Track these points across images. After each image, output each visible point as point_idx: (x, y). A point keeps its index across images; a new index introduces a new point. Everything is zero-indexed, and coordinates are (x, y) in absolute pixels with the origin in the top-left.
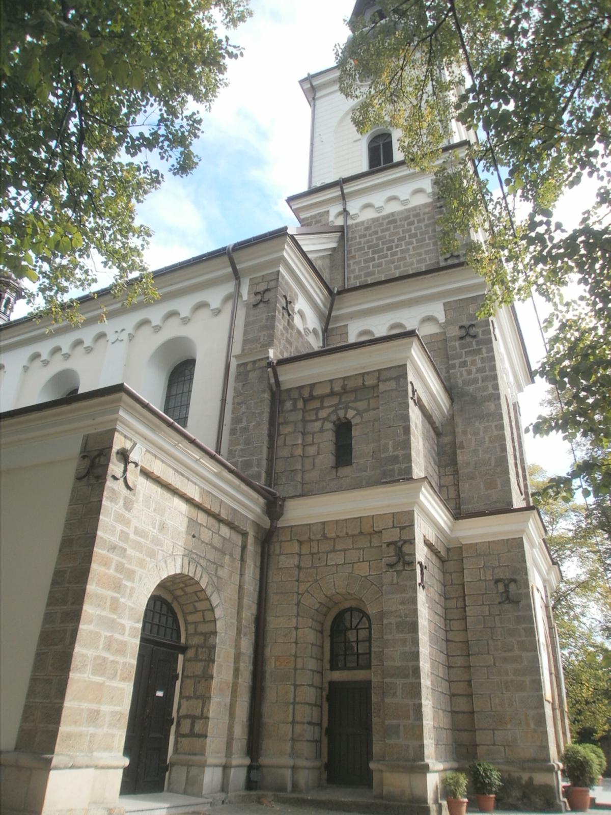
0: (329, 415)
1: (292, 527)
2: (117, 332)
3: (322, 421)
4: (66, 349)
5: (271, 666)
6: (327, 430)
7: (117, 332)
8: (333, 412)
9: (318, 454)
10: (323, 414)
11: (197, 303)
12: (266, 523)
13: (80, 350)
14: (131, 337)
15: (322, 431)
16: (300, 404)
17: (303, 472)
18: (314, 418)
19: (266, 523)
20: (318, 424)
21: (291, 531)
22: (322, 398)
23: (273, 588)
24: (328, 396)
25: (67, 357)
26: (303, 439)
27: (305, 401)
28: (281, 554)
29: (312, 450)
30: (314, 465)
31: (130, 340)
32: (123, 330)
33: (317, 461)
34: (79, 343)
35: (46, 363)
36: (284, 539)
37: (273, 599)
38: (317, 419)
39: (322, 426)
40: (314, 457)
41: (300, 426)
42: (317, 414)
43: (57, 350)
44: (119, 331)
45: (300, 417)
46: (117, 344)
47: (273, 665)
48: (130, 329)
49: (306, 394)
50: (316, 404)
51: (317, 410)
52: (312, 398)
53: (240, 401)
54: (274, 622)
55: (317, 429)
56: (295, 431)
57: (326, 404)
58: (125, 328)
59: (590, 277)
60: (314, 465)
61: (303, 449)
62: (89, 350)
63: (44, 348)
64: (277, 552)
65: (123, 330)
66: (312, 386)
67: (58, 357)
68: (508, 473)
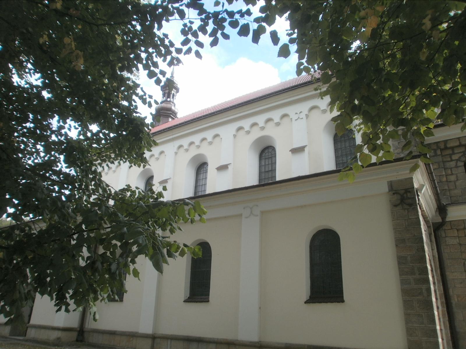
0: (460, 158)
1: (450, 221)
2: (296, 113)
3: (455, 161)
4: (197, 143)
5: (454, 300)
6: (460, 166)
7: (296, 113)
8: (462, 156)
9: (457, 180)
10: (455, 157)
11: (253, 123)
12: (439, 220)
13: (205, 143)
14: (307, 116)
15: (457, 167)
16: (439, 152)
17: (449, 190)
18: (449, 159)
19: (439, 220)
20: (453, 164)
21: (451, 224)
22: (452, 148)
23: (445, 256)
24: (456, 147)
25: (198, 147)
26: (445, 172)
27: (442, 150)
28: (446, 237)
29: (452, 178)
30: (456, 186)
31: (307, 118)
32: (301, 112)
33: (457, 183)
34: (204, 139)
35: (187, 150)
36: (446, 228)
37: (447, 263)
38: (452, 160)
39: (456, 164)
40: (455, 182)
41: (442, 164)
42: (451, 157)
43: (192, 143)
44: (299, 113)
45: (441, 159)
46: (299, 120)
47: (456, 300)
48: (306, 112)
49: (442, 147)
50: (450, 152)
51: (450, 155)
52: (446, 148)
53: (399, 152)
54: (450, 276)
55: (454, 166)
56: (439, 167)
57: (456, 151)
58: (302, 111)
59: (19, 235)
60: (456, 186)
61: (446, 178)
62: (211, 143)
63: (185, 142)
64: (444, 235)
65: (301, 112)
66: (446, 142)
67: (193, 147)
68: (420, 225)
